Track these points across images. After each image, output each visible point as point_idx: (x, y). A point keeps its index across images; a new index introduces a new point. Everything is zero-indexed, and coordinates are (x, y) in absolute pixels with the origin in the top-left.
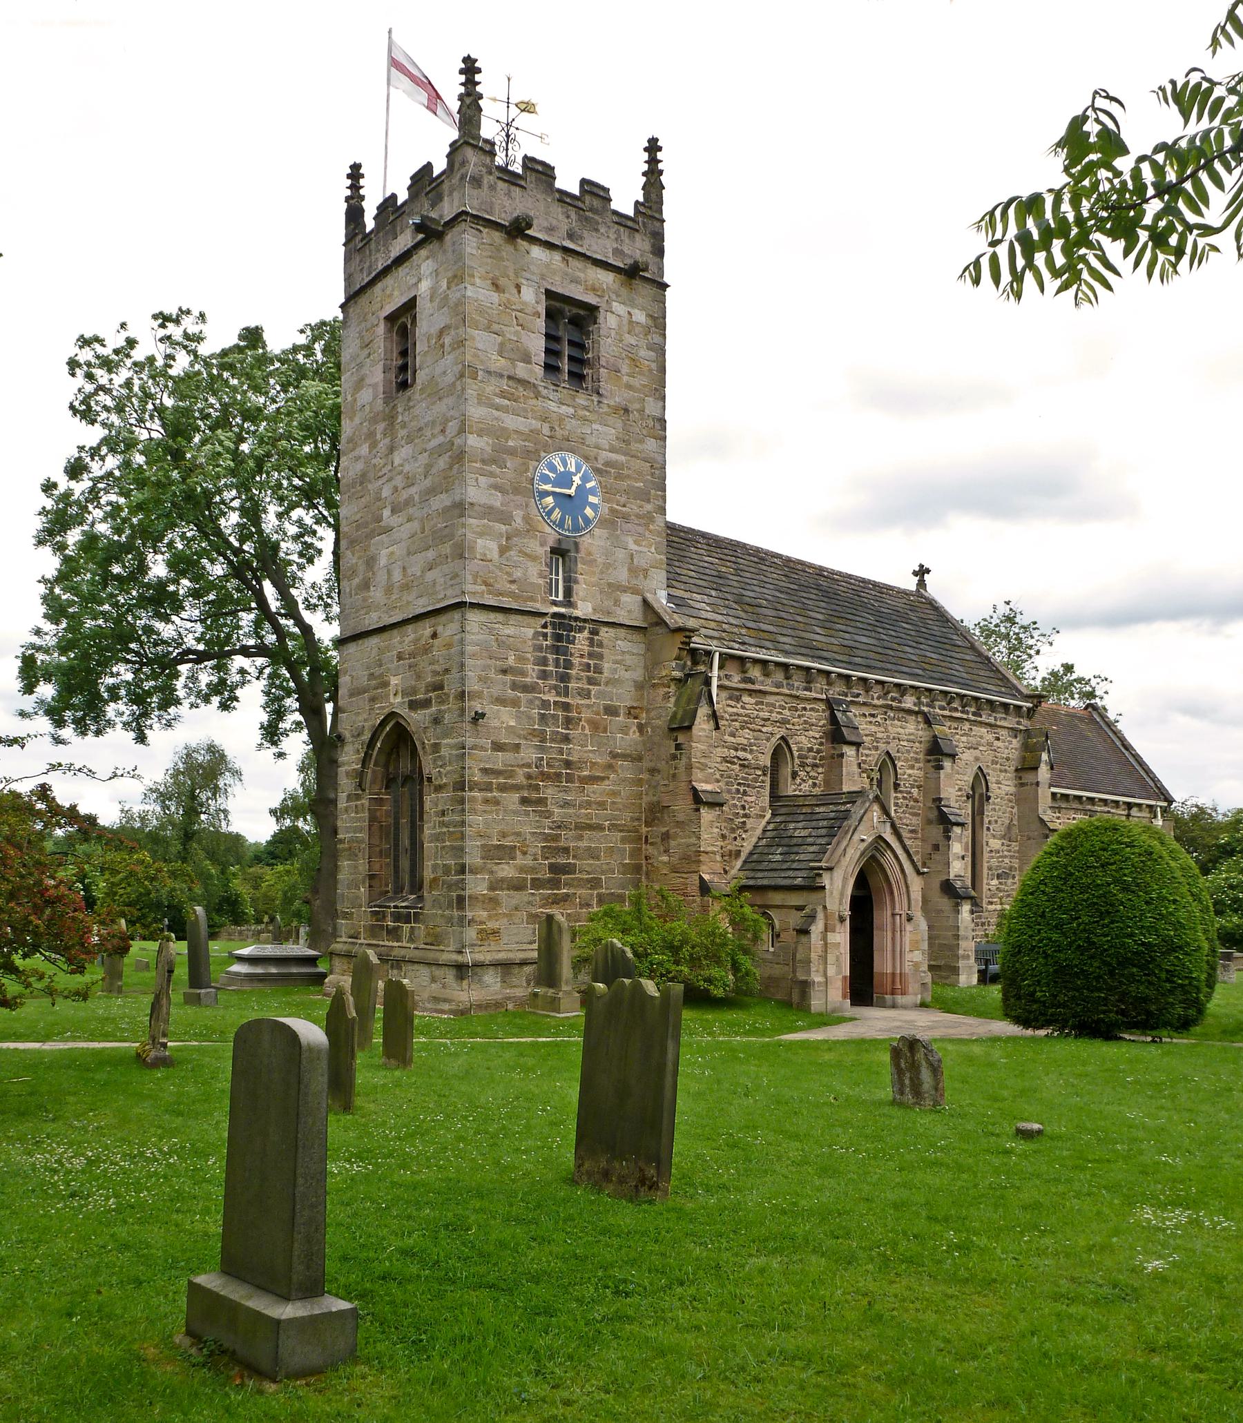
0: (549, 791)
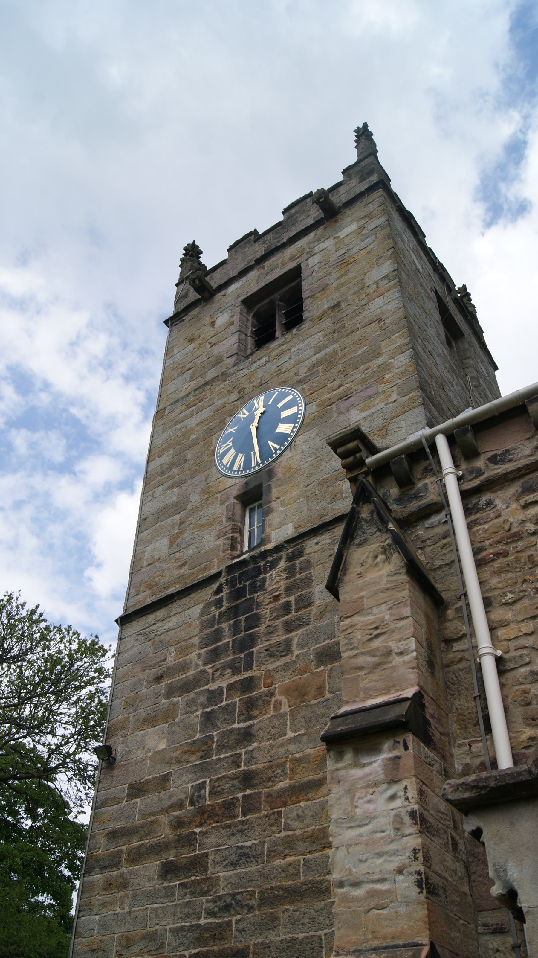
0: (212, 839)
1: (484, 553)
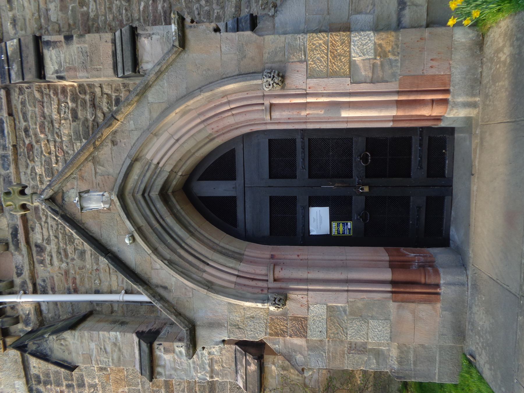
1: (71, 288)
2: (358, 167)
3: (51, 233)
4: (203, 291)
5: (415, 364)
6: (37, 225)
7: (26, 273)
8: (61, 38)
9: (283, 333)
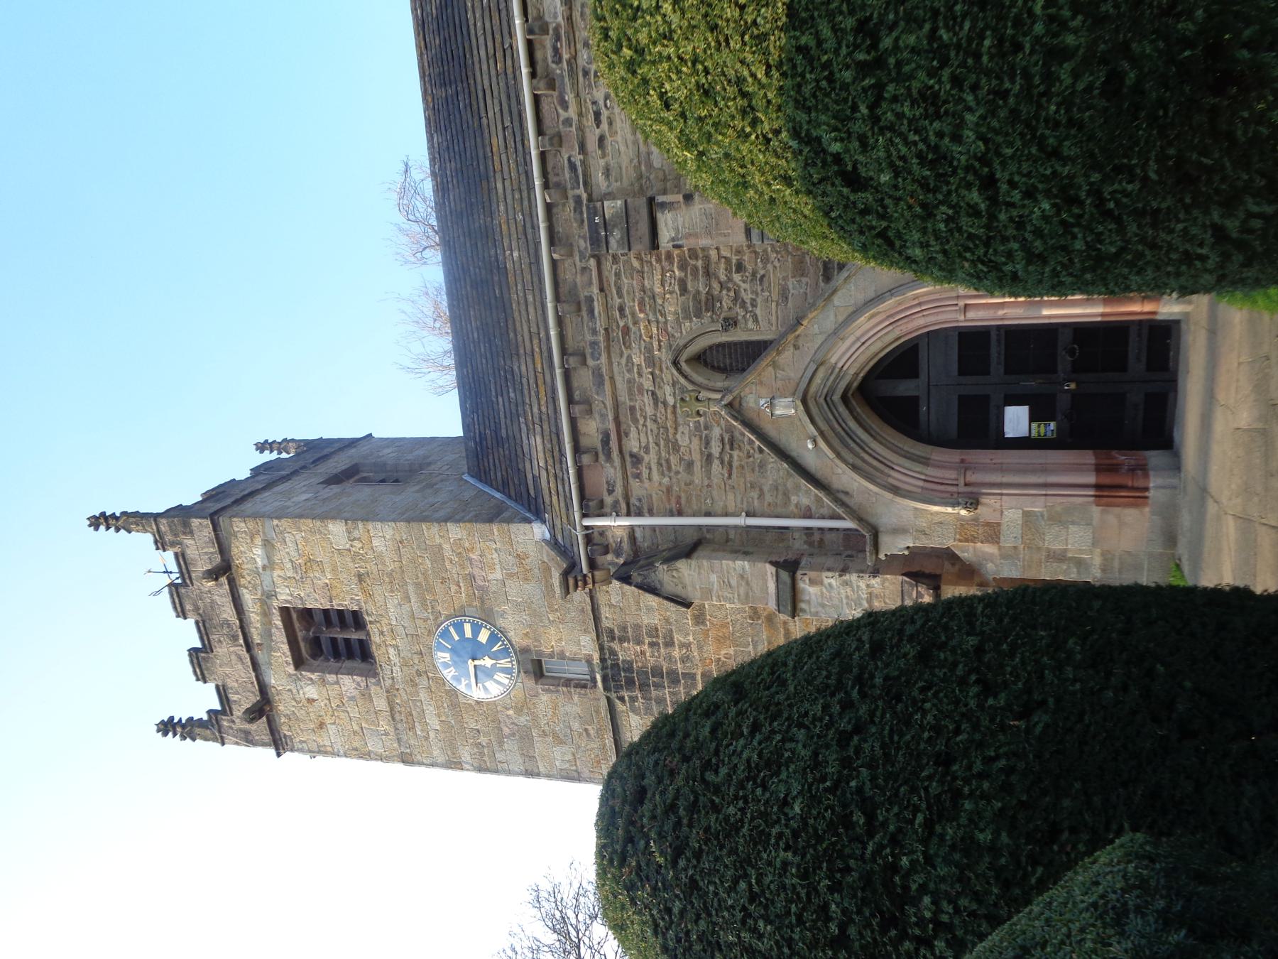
2: (1064, 361)
3: (651, 439)
4: (889, 496)
5: (1120, 572)
6: (633, 429)
7: (619, 490)
8: (680, 198)
9: (973, 539)
